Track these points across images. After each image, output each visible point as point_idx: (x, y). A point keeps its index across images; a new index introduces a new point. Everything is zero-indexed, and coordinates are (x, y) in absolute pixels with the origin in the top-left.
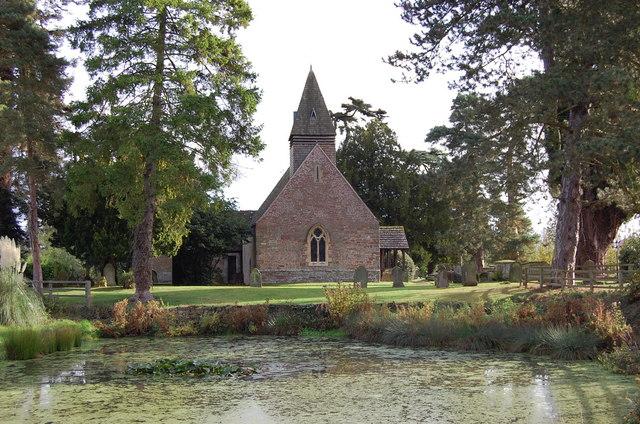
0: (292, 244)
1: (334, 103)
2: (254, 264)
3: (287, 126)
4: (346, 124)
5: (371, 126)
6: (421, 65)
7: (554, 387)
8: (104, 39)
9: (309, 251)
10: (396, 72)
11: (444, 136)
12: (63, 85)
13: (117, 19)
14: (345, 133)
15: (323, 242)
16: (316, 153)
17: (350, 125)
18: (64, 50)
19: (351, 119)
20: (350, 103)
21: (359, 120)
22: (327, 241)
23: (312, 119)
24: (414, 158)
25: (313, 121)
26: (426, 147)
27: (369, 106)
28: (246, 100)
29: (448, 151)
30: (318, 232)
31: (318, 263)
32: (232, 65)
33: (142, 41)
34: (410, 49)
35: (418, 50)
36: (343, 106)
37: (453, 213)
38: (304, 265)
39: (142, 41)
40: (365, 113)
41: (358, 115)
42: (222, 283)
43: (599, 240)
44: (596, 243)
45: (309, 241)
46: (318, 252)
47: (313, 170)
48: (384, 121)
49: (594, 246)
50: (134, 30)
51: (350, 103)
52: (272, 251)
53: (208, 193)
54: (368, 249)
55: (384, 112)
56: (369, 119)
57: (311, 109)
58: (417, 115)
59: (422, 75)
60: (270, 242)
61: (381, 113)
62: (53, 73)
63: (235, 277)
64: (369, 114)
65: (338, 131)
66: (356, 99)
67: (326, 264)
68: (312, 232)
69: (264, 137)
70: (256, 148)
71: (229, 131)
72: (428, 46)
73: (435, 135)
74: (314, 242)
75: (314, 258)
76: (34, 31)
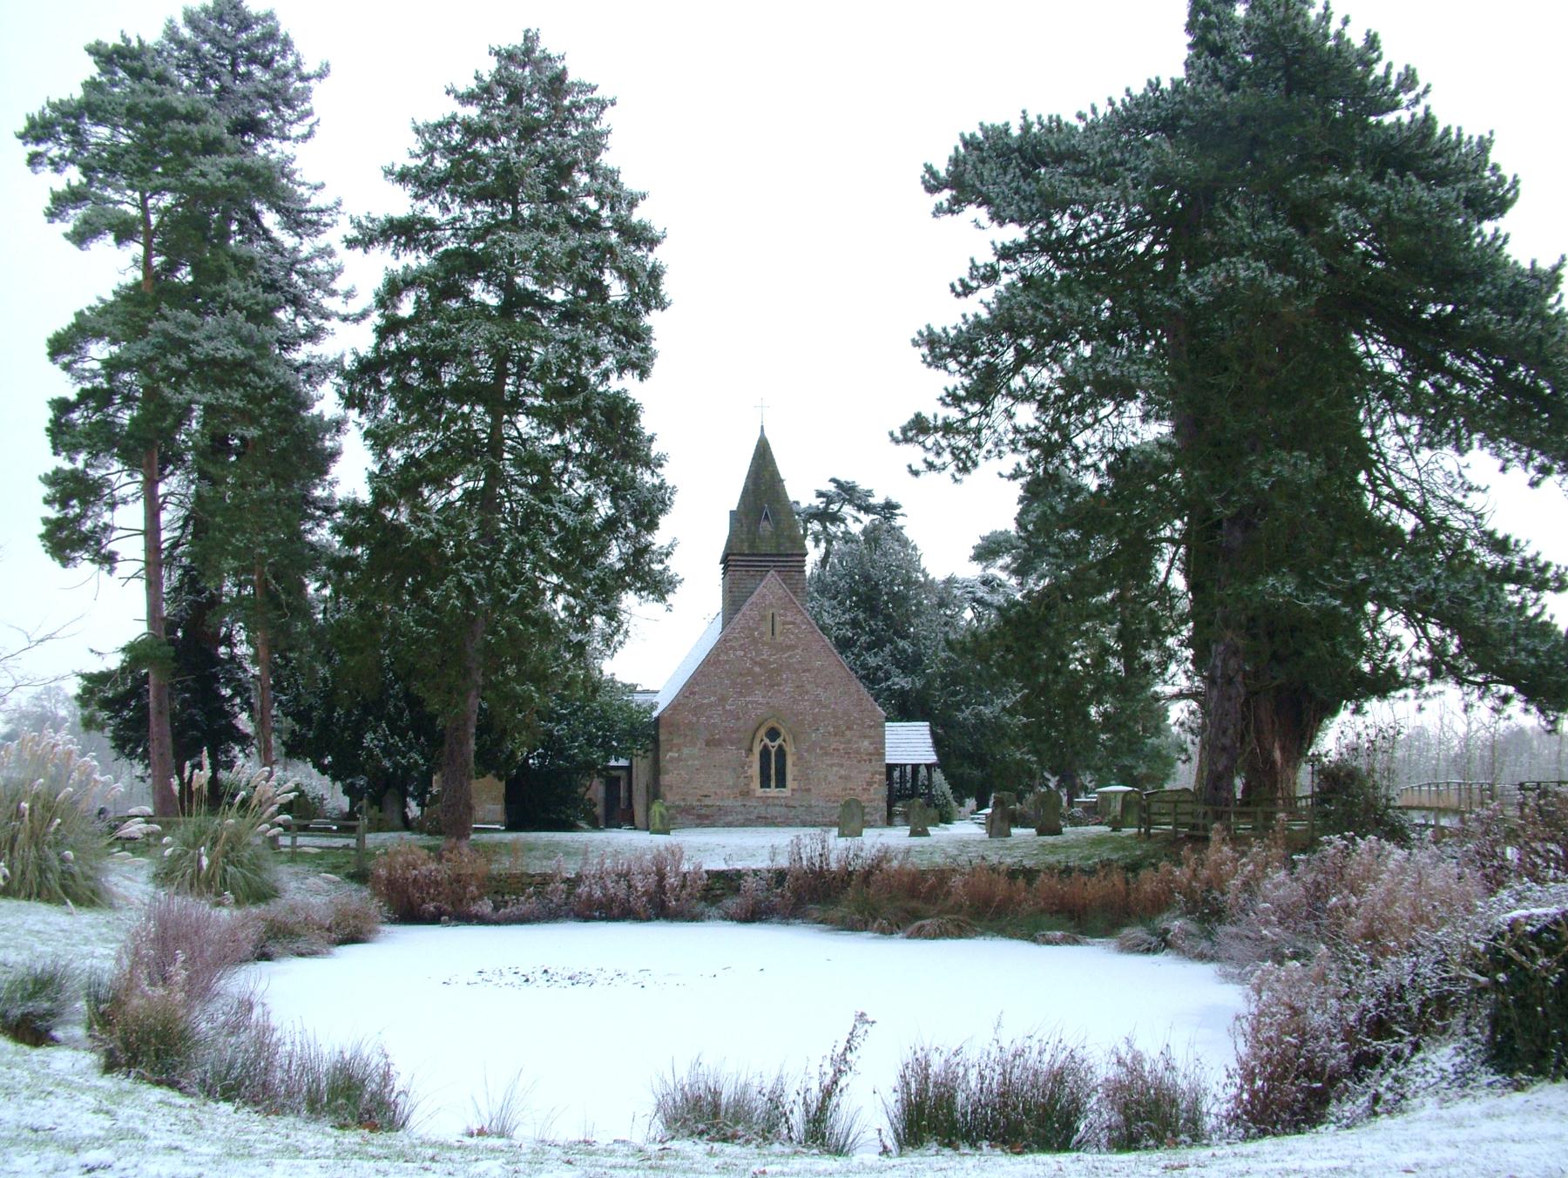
0: (731, 753)
1: (802, 490)
2: (654, 793)
3: (718, 535)
4: (825, 528)
5: (871, 535)
6: (961, 442)
7: (1246, 1026)
8: (402, 388)
9: (755, 770)
10: (914, 454)
11: (1008, 551)
12: (321, 462)
13: (421, 352)
14: (823, 545)
15: (781, 753)
16: (770, 586)
17: (832, 529)
18: (327, 401)
19: (835, 518)
20: (832, 488)
21: (850, 521)
22: (790, 750)
23: (764, 525)
24: (946, 594)
25: (766, 527)
26: (972, 572)
27: (869, 493)
28: (647, 509)
29: (1013, 581)
30: (773, 734)
31: (773, 791)
32: (617, 434)
33: (466, 392)
34: (936, 411)
35: (954, 414)
36: (820, 494)
37: (1162, 336)
38: (746, 793)
39: (466, 392)
40: (860, 508)
41: (848, 510)
42: (595, 825)
43: (1282, 749)
44: (1277, 755)
45: (757, 749)
46: (773, 770)
47: (763, 618)
48: (898, 522)
49: (1274, 762)
50: (449, 376)
51: (832, 488)
52: (685, 769)
53: (162, 258)
54: (866, 766)
55: (897, 507)
56: (867, 519)
57: (763, 508)
58: (957, 526)
59: (965, 464)
60: (686, 751)
61: (890, 508)
62: (308, 453)
63: (619, 815)
64: (868, 509)
65: (809, 543)
66: (842, 479)
67: (786, 792)
68: (763, 731)
69: (675, 565)
70: (659, 587)
71: (615, 555)
72: (975, 408)
73: (987, 551)
74: (765, 753)
75: (765, 783)
76: (595, 687)
